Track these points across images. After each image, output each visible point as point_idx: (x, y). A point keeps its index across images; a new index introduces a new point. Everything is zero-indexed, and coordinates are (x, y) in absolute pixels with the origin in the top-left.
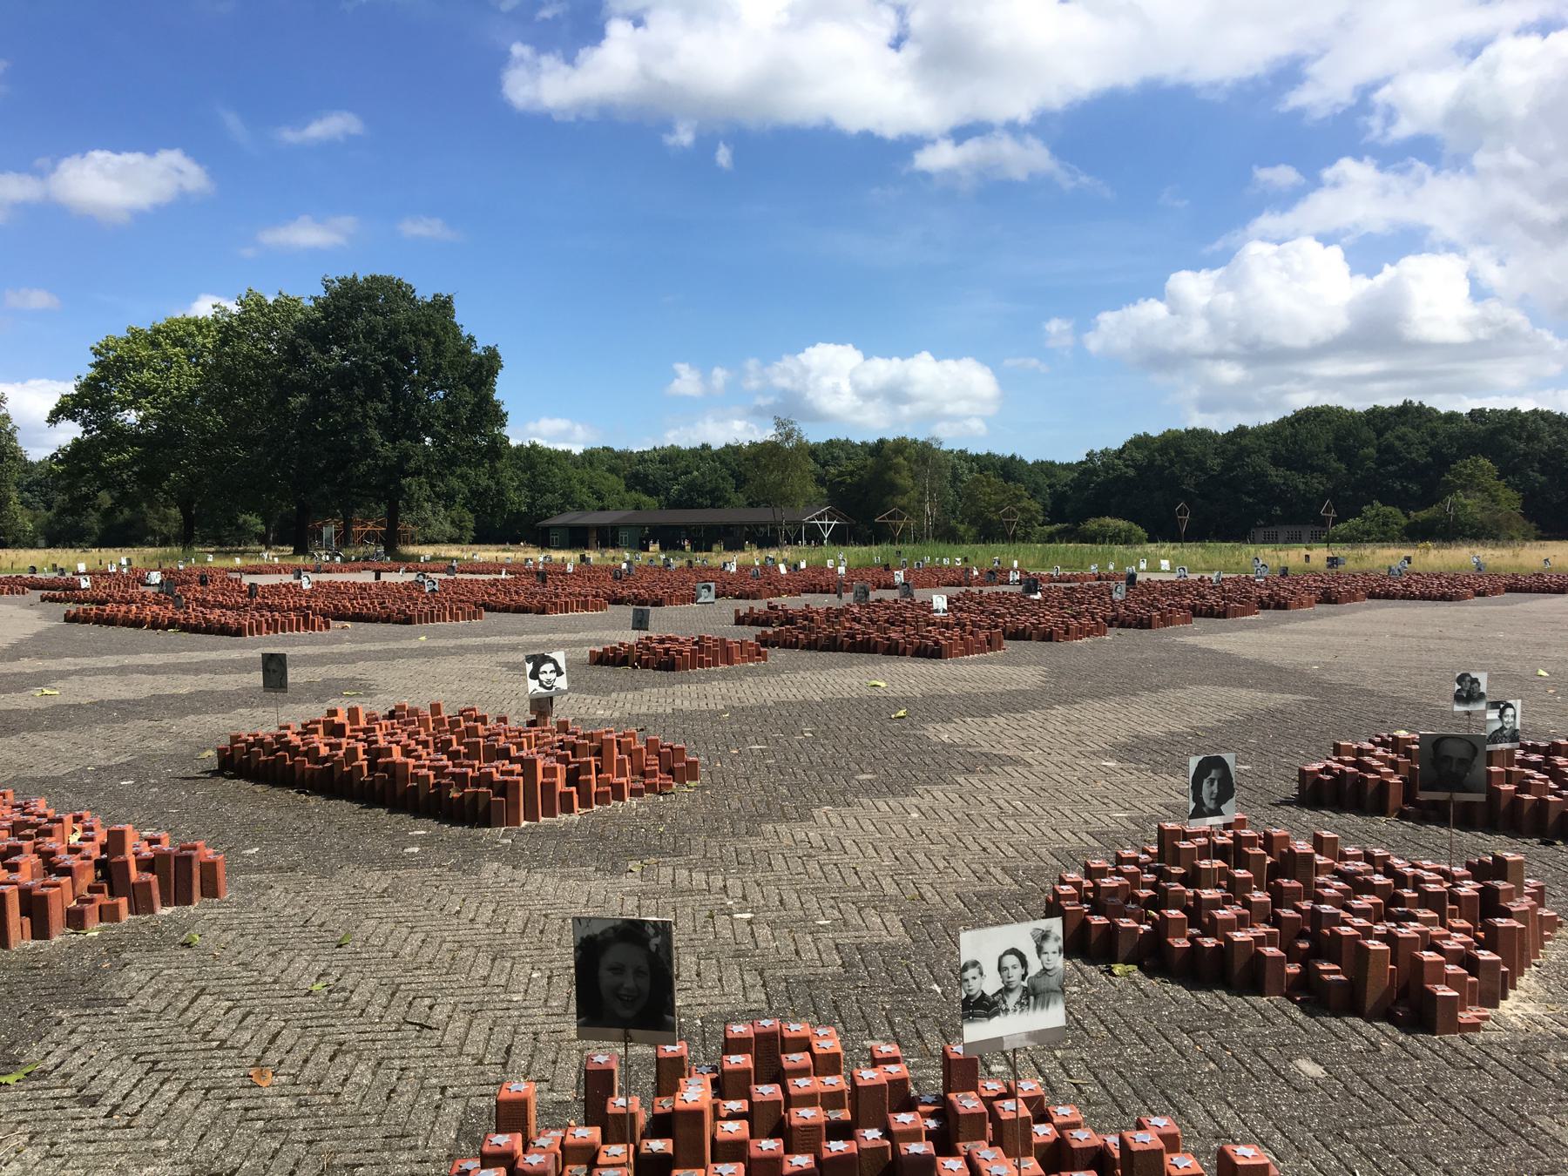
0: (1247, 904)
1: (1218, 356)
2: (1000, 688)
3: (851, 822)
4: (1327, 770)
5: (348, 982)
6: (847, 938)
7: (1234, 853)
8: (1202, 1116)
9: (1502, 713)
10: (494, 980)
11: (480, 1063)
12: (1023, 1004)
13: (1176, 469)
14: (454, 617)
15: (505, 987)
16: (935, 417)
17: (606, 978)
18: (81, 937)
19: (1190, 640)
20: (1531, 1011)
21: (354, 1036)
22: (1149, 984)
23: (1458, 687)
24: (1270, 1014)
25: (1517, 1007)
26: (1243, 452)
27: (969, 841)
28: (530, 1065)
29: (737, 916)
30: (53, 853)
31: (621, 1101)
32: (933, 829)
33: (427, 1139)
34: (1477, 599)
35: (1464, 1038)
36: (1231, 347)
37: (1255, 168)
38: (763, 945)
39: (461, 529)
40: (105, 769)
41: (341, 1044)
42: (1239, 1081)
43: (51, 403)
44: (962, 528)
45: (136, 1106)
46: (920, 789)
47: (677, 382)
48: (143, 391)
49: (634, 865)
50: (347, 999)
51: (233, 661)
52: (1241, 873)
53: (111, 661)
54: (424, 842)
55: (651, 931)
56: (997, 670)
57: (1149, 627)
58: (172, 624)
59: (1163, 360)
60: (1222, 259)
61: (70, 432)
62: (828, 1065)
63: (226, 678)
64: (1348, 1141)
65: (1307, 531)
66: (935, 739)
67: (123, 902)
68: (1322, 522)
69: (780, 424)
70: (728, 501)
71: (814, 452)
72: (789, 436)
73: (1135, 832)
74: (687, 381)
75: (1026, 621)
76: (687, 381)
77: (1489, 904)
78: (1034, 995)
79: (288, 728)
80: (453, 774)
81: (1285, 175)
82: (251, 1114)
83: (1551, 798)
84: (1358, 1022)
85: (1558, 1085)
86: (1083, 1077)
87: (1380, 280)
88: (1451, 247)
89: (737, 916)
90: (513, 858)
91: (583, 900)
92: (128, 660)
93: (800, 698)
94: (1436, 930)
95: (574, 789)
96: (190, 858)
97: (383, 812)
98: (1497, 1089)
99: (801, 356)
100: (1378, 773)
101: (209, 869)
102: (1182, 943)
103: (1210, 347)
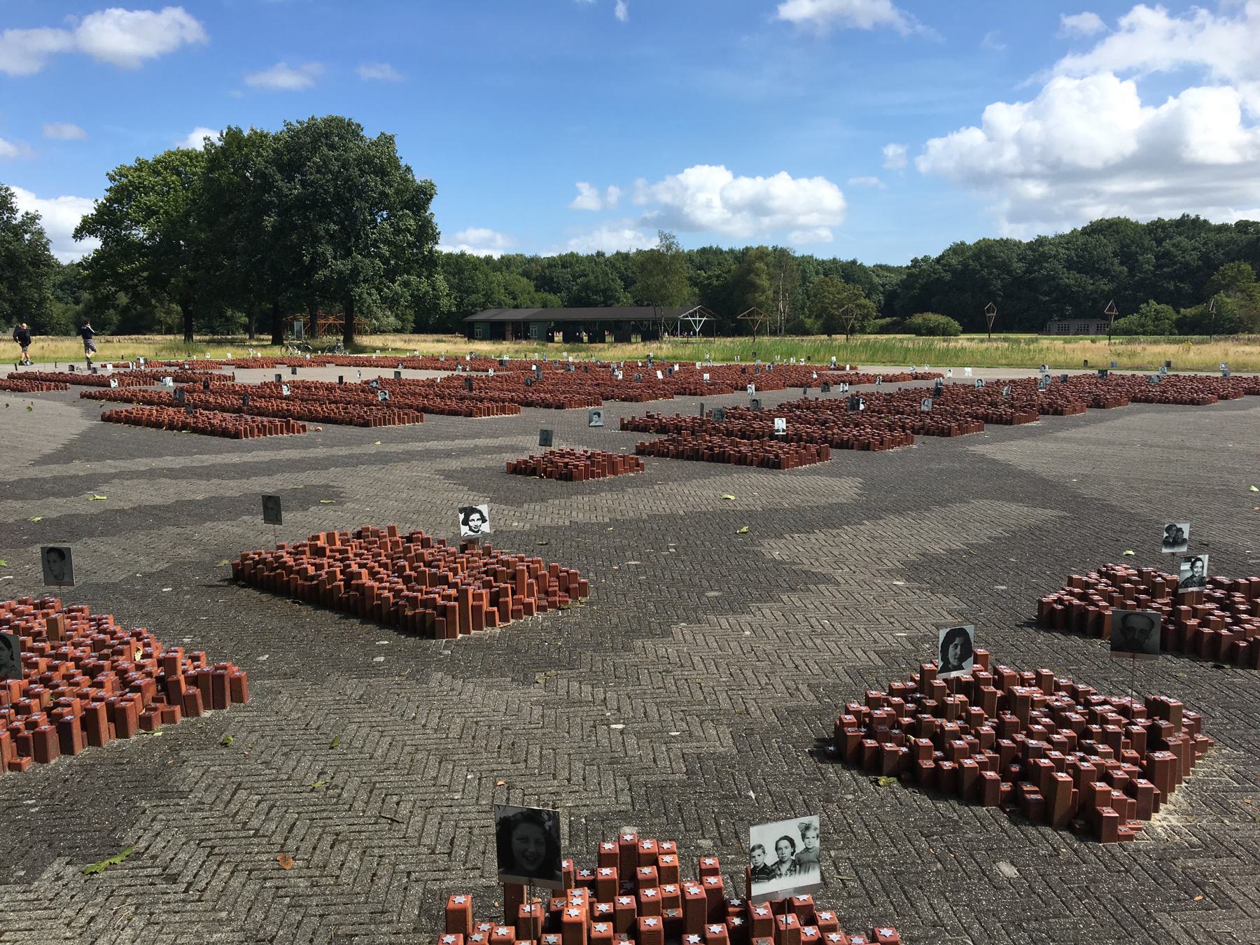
0: (978, 735)
1: (1025, 176)
2: (823, 501)
3: (699, 637)
4: (1059, 601)
5: (339, 780)
6: (690, 748)
7: (972, 689)
8: (927, 908)
9: (1193, 565)
10: (441, 781)
11: (433, 852)
12: (791, 871)
13: (985, 272)
14: (402, 421)
15: (449, 786)
16: (790, 227)
17: (517, 845)
18: (150, 737)
19: (980, 449)
20: (1174, 822)
21: (346, 828)
22: (904, 793)
23: (1166, 535)
24: (986, 823)
25: (1164, 819)
26: (1044, 257)
27: (786, 658)
28: (467, 855)
29: (613, 726)
30: (126, 671)
31: (527, 908)
32: (761, 646)
33: (399, 915)
34: (1221, 403)
35: (1121, 845)
36: (1037, 168)
37: (1062, 15)
38: (630, 753)
39: (403, 321)
40: (150, 575)
41: (337, 835)
42: (956, 879)
43: (77, 222)
44: (809, 322)
45: (203, 884)
46: (753, 606)
47: (579, 198)
48: (150, 212)
49: (540, 677)
50: (339, 795)
51: (235, 465)
52: (976, 710)
53: (142, 464)
54: (387, 651)
55: (546, 817)
56: (823, 481)
57: (949, 435)
58: (185, 426)
59: (981, 179)
60: (1030, 95)
61: (93, 244)
62: (669, 875)
63: (232, 483)
64: (1024, 930)
65: (1093, 325)
66: (768, 556)
67: (177, 709)
68: (1107, 318)
69: (663, 237)
70: (618, 300)
71: (689, 257)
72: (669, 248)
73: (910, 652)
74: (587, 198)
75: (851, 432)
76: (587, 198)
77: (1154, 739)
78: (799, 864)
79: (282, 547)
80: (407, 597)
81: (1089, 22)
82: (281, 892)
83: (1224, 632)
84: (1048, 831)
85: (1179, 887)
86: (848, 874)
87: (1164, 109)
88: (1225, 82)
89: (613, 726)
90: (451, 668)
91: (503, 708)
92: (156, 463)
93: (668, 511)
94: (1111, 762)
95: (495, 609)
96: (222, 676)
97: (356, 621)
98: (1136, 890)
99: (680, 176)
100: (1097, 606)
101: (236, 683)
102: (928, 764)
103: (1020, 168)
